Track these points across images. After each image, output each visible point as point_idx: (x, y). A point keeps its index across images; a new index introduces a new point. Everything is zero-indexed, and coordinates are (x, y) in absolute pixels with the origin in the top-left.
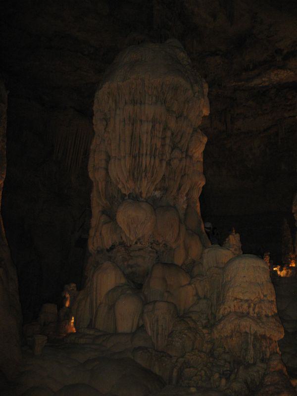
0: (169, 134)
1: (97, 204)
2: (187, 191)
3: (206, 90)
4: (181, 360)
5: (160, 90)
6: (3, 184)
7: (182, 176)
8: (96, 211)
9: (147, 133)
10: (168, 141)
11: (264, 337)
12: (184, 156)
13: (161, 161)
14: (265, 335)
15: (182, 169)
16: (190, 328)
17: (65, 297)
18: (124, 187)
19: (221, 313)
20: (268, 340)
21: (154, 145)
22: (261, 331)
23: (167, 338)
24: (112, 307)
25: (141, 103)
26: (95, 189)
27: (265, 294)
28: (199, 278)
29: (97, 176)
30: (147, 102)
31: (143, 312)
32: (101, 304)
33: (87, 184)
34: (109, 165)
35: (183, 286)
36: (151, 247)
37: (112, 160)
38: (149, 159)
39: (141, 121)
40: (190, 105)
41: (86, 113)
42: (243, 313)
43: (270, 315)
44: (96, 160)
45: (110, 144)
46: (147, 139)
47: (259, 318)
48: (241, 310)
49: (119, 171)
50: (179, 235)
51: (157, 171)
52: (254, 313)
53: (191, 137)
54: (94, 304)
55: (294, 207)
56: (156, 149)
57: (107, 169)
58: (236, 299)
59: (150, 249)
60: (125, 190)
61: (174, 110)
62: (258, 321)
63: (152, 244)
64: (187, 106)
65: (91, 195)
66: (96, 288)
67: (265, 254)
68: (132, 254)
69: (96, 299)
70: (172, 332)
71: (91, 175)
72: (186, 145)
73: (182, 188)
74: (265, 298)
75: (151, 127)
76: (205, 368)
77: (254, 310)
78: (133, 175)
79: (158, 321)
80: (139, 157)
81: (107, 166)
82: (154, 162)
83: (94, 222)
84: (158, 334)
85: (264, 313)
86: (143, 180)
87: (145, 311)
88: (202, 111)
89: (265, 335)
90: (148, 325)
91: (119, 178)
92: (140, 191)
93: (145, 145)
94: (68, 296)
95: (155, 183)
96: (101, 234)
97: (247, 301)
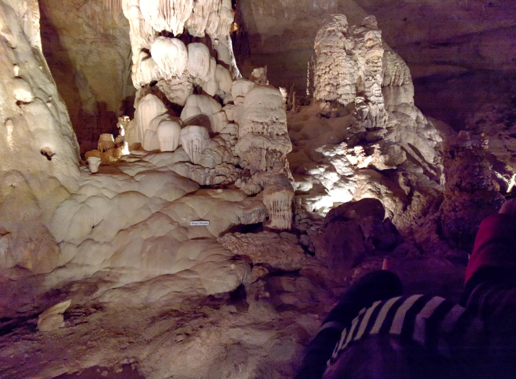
2: (216, 28)
4: (213, 170)
6: (75, 134)
11: (275, 151)
14: (275, 150)
16: (219, 147)
17: (120, 128)
20: (358, 182)
22: (272, 147)
24: (155, 133)
27: (277, 117)
28: (228, 107)
31: (180, 136)
32: (147, 130)
36: (188, 81)
43: (280, 134)
47: (271, 136)
48: (257, 131)
50: (210, 69)
54: (142, 132)
55: (315, 43)
58: (253, 122)
59: (188, 83)
62: (270, 139)
63: (188, 78)
66: (142, 117)
68: (173, 88)
74: (277, 121)
76: (232, 176)
77: (267, 130)
78: (163, 12)
85: (275, 133)
89: (275, 150)
94: (122, 127)
95: (185, 20)
97: (262, 123)
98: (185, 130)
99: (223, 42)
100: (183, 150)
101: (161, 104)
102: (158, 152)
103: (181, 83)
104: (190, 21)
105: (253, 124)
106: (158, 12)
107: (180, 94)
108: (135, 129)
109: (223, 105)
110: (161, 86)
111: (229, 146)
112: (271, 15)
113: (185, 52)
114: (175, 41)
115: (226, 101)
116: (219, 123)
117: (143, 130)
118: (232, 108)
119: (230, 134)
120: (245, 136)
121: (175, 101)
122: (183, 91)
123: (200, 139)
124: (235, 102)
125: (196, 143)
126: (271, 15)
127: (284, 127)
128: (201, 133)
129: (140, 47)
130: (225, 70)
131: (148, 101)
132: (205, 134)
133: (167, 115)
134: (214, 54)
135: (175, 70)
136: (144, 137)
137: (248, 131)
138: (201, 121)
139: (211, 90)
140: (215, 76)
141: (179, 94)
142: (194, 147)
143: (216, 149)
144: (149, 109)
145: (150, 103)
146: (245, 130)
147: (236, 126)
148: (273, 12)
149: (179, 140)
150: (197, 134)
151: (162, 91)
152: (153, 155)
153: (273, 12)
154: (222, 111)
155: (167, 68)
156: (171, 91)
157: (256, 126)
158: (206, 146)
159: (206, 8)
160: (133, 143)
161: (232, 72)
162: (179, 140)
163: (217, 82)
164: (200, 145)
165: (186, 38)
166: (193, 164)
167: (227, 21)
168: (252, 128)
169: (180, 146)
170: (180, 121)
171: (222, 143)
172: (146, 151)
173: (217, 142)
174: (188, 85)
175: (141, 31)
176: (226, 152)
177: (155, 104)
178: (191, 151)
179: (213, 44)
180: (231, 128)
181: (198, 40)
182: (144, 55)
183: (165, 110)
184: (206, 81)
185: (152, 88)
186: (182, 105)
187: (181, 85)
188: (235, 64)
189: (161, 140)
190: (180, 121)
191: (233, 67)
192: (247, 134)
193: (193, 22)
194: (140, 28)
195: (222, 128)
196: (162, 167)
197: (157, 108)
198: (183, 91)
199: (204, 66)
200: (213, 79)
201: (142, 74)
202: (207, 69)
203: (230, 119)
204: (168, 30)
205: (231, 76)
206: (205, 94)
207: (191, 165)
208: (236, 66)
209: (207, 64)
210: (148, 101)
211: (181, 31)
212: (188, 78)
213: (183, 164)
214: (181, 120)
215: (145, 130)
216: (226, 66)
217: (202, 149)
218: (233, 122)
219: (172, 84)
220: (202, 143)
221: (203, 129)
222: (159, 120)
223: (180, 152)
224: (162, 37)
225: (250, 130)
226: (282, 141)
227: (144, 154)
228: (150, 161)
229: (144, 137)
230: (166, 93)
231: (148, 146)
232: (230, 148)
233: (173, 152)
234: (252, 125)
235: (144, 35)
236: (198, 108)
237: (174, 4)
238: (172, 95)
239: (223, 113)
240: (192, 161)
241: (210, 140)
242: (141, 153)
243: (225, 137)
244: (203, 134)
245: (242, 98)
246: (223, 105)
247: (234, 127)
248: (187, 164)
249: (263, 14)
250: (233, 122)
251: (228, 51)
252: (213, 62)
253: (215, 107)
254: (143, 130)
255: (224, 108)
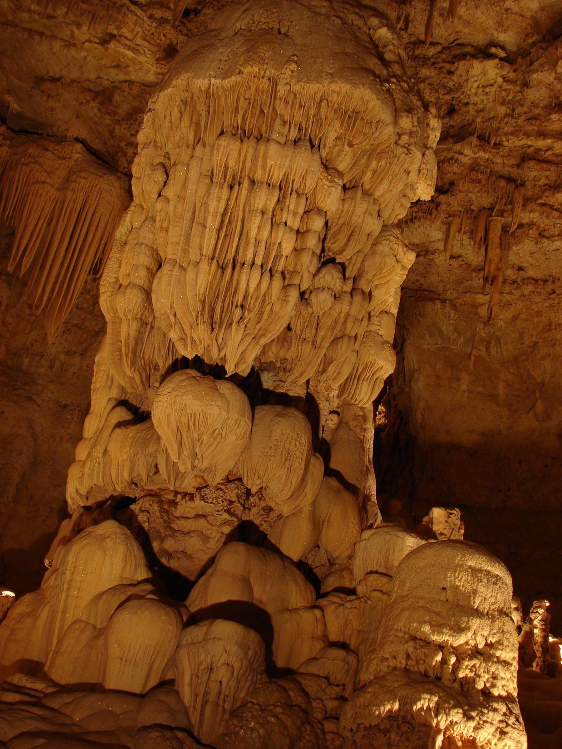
0: (318, 224)
1: (109, 376)
2: (342, 380)
3: (435, 136)
5: (312, 112)
7: (336, 340)
8: (101, 400)
9: (263, 213)
10: (312, 242)
12: (348, 287)
13: (285, 287)
15: (336, 322)
16: (289, 706)
18: (183, 340)
19: (372, 668)
21: (276, 247)
23: (227, 717)
24: (101, 632)
25: (259, 139)
26: (108, 339)
28: (336, 600)
29: (118, 305)
30: (275, 136)
31: (178, 646)
33: (90, 328)
34: (156, 281)
35: (290, 611)
36: (228, 511)
37: (166, 268)
38: (259, 277)
39: (253, 182)
40: (383, 163)
41: (112, 160)
42: (426, 675)
44: (124, 266)
45: (167, 231)
46: (259, 228)
48: (422, 668)
49: (179, 296)
50: (303, 480)
51: (271, 311)
52: (455, 681)
53: (374, 245)
54: (58, 625)
56: (278, 257)
57: (147, 293)
58: (414, 638)
59: (226, 516)
60: (186, 345)
61: (341, 167)
64: (374, 164)
65: (97, 359)
66: (70, 582)
67: (535, 604)
68: (178, 525)
69: (64, 612)
70: (244, 705)
71: (104, 302)
72: (359, 261)
73: (331, 369)
75: (275, 199)
78: (212, 310)
79: (212, 669)
80: (234, 268)
81: (151, 283)
82: (269, 288)
83: (91, 426)
84: (205, 702)
86: (234, 326)
87: (184, 642)
88: (413, 188)
90: (187, 680)
91: (175, 315)
92: (222, 355)
93: (252, 241)
95: (264, 341)
96: (106, 451)
98: (196, 633)
99: (352, 424)
100: (177, 693)
101: (138, 552)
102: (94, 688)
103: (204, 516)
104: (274, 348)
105: (411, 644)
106: (199, 306)
107: (197, 535)
108: (36, 619)
109: (320, 595)
110: (146, 513)
111: (319, 716)
112: (493, 397)
113: (246, 421)
114: (226, 388)
115: (330, 584)
116: (299, 631)
117: (63, 621)
118: (348, 605)
119: (327, 678)
120: (379, 679)
121: (173, 564)
122: (206, 539)
123: (237, 666)
124: (360, 590)
125: (222, 674)
126: (493, 397)
127: (508, 676)
128: (244, 646)
129: (115, 393)
130: (347, 497)
131: (104, 538)
132: (255, 653)
133: (149, 587)
134: (321, 448)
135: (205, 464)
136: (60, 641)
137: (392, 663)
138: (250, 615)
139: (294, 544)
140: (314, 504)
141: (193, 544)
142: (214, 688)
143: (279, 710)
144: (97, 564)
145: (109, 543)
146: (384, 659)
147: (351, 659)
148: (501, 389)
149: (173, 662)
150: (234, 649)
151: (146, 525)
152: (79, 695)
153: (501, 389)
154: (314, 607)
155: (186, 452)
156: (169, 533)
157: (421, 652)
158: (247, 694)
159: (327, 322)
160: (18, 657)
161: (362, 509)
162: (173, 662)
163: (317, 524)
164: (233, 684)
165: (255, 390)
166: (198, 742)
167: (374, 369)
168: (408, 656)
169: (167, 685)
170: (182, 609)
171: (297, 698)
172: (55, 684)
173: (286, 690)
174: (224, 523)
175: (134, 352)
176: (308, 728)
177: (121, 549)
178: (199, 700)
179: (322, 423)
180: (335, 663)
181: (284, 400)
182: (122, 414)
183: (143, 574)
184: (285, 514)
185: (118, 508)
186: (192, 578)
187: (202, 521)
188: (374, 492)
189: (115, 651)
190: (182, 609)
191: (367, 498)
192: (387, 673)
193: (282, 354)
194: (136, 344)
195: (303, 659)
196: (98, 732)
197: (125, 562)
198: (206, 539)
199: (290, 468)
200: (306, 511)
201: (100, 462)
202: (295, 480)
203: (334, 637)
204: (213, 357)
205: (361, 520)
206: (275, 550)
207: (189, 742)
208: (374, 499)
209: (299, 465)
210: (104, 538)
211: (244, 371)
212: (231, 502)
213: (168, 734)
214: (187, 608)
215: (70, 618)
216: (352, 489)
217: (235, 699)
218: (343, 646)
219: (177, 513)
220: (238, 681)
221: (253, 638)
222: (123, 598)
223: (164, 698)
224: (192, 372)
225: (401, 662)
226: (498, 717)
227: (50, 690)
228: (67, 711)
229: (60, 641)
230: (152, 534)
231: (63, 672)
232: (319, 722)
233: (141, 696)
234: (410, 646)
235: (140, 363)
236: (246, 582)
237: (245, 297)
238: (170, 545)
239: (317, 612)
240: (196, 734)
241: (264, 677)
242: (40, 686)
243: (311, 687)
244: (250, 653)
245: (384, 580)
246: (320, 595)
247: (344, 660)
248: (180, 735)
249: (470, 391)
250: (343, 646)
251: (363, 448)
252: (318, 467)
253: (297, 594)
254: (63, 621)
255: (323, 602)
